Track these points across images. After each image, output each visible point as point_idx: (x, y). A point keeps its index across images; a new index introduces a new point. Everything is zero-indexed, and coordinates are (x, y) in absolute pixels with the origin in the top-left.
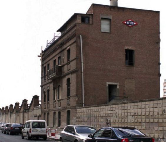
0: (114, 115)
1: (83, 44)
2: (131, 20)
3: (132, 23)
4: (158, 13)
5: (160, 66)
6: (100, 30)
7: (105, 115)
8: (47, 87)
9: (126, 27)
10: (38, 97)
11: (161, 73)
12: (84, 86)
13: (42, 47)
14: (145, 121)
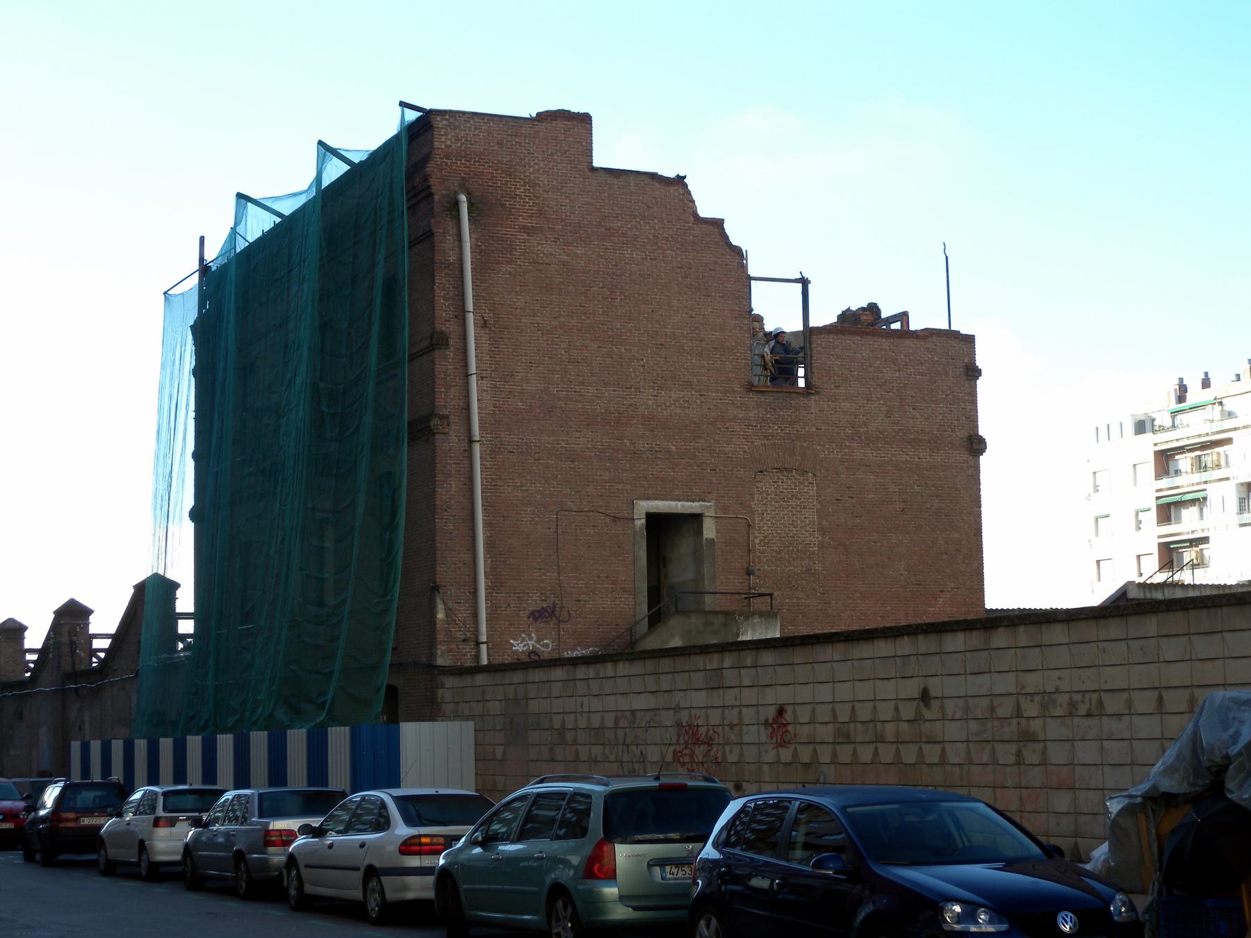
1: (475, 248)
5: (980, 383)
7: (617, 719)
10: (174, 586)
13: (202, 240)
14: (835, 754)
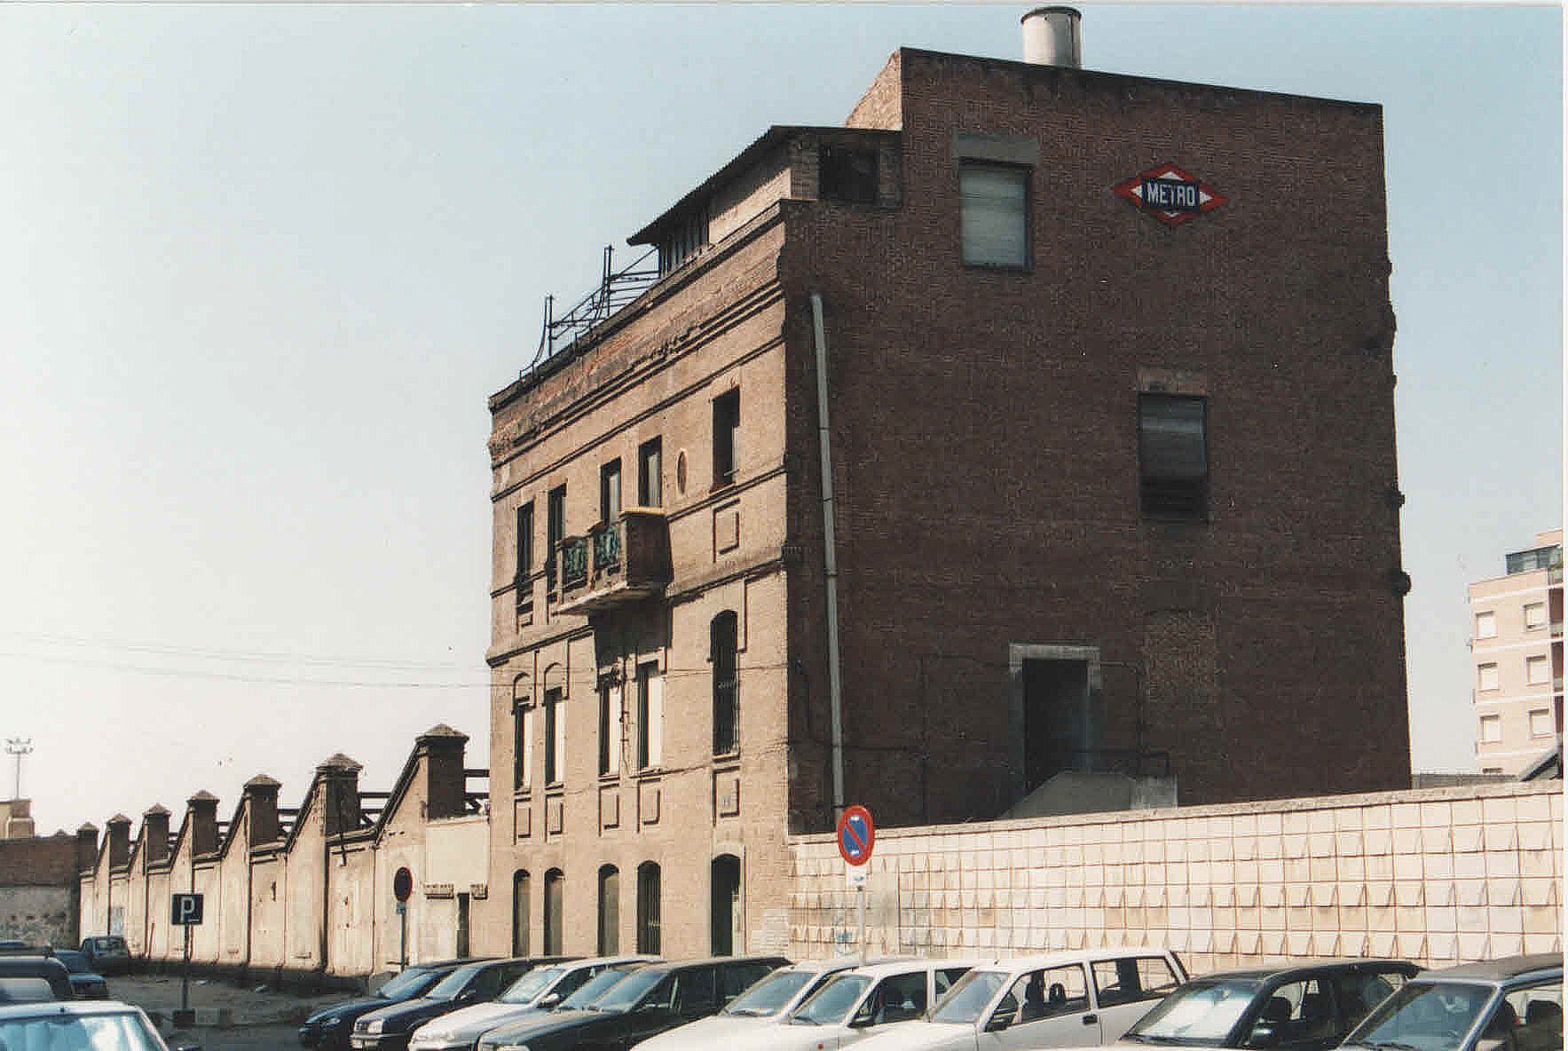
0: (1074, 898)
1: (831, 358)
2: (1177, 171)
3: (1184, 195)
4: (1370, 115)
6: (958, 248)
8: (541, 668)
9: (1144, 226)
11: (1406, 567)
12: (843, 671)
